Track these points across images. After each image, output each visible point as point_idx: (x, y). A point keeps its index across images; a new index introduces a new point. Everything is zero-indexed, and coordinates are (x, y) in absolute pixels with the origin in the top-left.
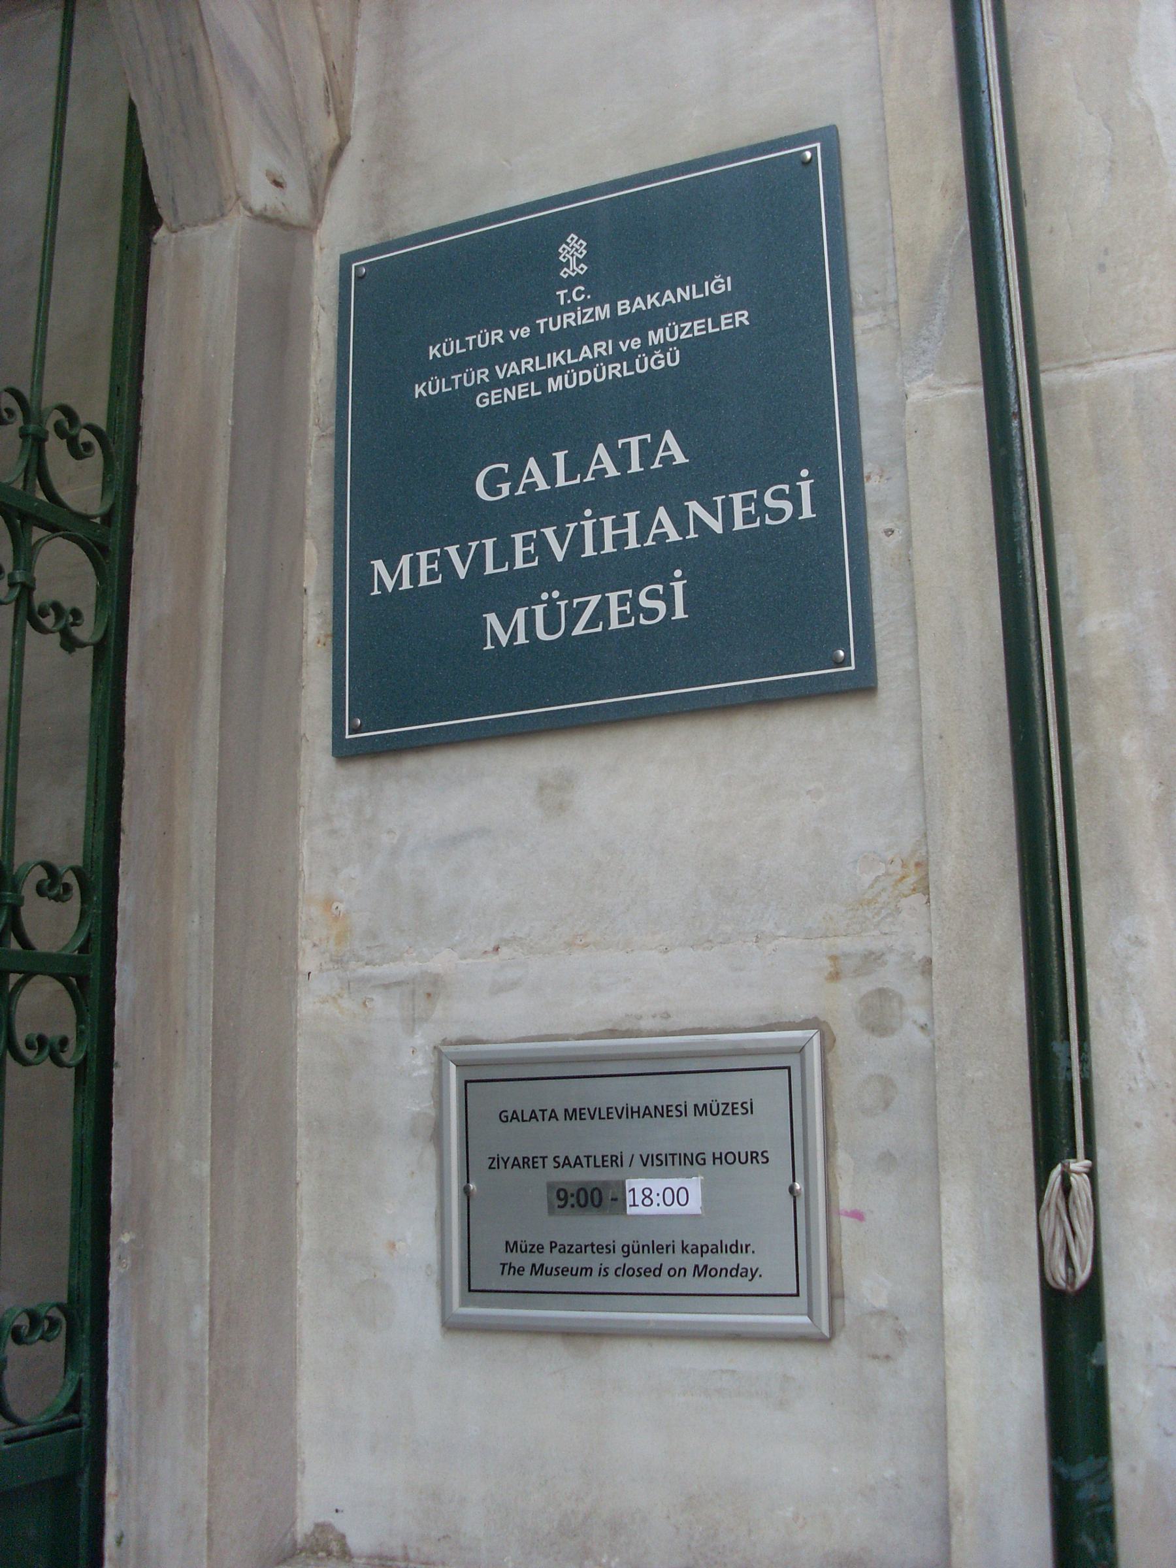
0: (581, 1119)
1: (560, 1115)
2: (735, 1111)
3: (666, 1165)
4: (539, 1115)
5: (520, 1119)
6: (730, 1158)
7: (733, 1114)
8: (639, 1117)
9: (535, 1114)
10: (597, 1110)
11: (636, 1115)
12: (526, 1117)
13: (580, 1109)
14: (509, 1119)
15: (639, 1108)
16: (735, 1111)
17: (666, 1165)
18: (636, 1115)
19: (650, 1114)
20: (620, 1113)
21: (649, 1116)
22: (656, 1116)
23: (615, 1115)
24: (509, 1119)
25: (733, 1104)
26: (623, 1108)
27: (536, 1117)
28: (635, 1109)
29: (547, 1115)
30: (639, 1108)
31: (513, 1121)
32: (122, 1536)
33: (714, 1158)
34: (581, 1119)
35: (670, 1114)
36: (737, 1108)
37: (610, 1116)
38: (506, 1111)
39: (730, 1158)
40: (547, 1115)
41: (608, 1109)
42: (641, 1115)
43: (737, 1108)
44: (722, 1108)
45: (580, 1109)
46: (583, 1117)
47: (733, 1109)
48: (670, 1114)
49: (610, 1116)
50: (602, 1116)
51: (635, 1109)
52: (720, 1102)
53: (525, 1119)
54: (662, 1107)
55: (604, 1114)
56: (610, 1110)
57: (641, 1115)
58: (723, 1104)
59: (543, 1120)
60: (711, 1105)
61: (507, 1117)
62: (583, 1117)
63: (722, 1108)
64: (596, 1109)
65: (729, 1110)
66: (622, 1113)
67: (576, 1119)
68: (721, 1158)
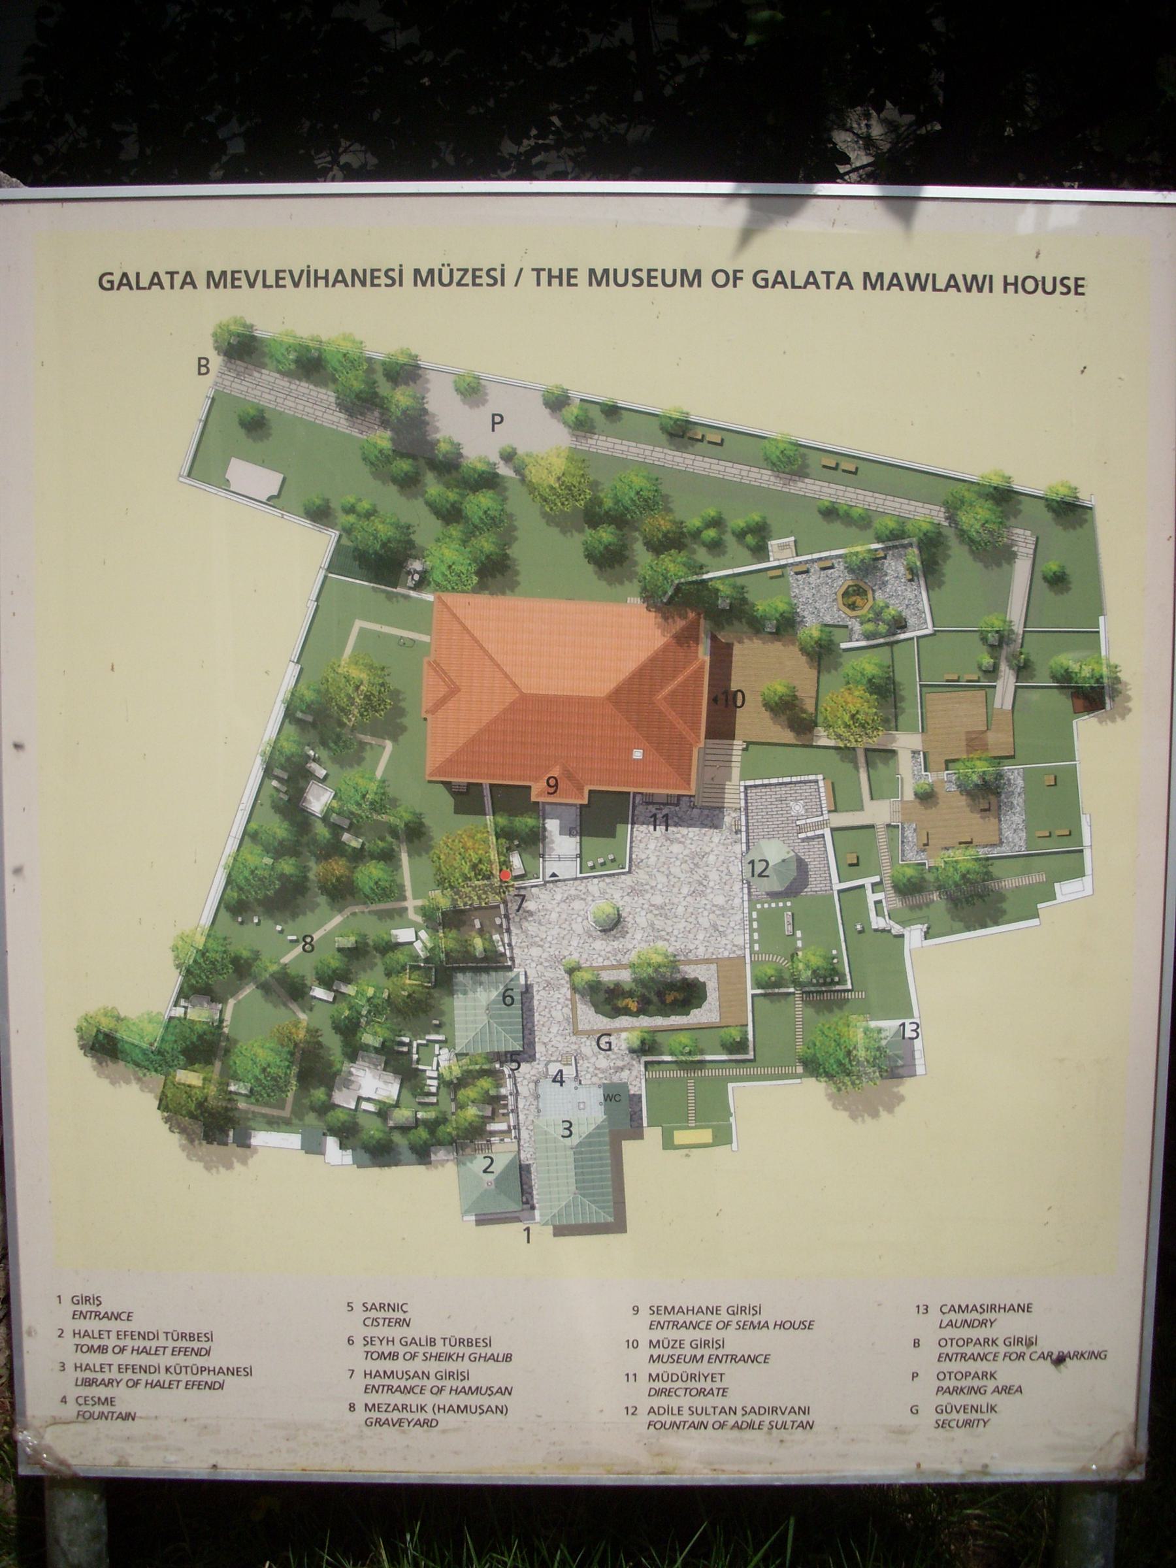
0: (569, 284)
1: (857, 281)
2: (478, 281)
3: (1055, 279)
4: (166, 280)
5: (134, 284)
6: (1030, 285)
7: (474, 284)
8: (327, 285)
9: (815, 278)
10: (261, 274)
11: (321, 283)
12: (144, 282)
13: (233, 273)
14: (770, 283)
15: (327, 271)
16: (478, 281)
17: (1055, 279)
18: (321, 283)
19: (344, 281)
20: (296, 280)
21: (127, 288)
22: (353, 285)
23: (288, 282)
24: (770, 283)
25: (474, 270)
26: (302, 271)
27: (816, 283)
28: (321, 274)
29: (834, 280)
30: (327, 271)
31: (122, 288)
32: (1037, 257)
33: (1006, 284)
34: (233, 286)
35: (376, 281)
36: (379, 277)
37: (281, 282)
38: (766, 272)
39: (1030, 285)
40: (834, 280)
41: (277, 272)
42: (331, 282)
43: (379, 277)
44: (457, 275)
45: (233, 273)
46: (237, 283)
47: (474, 277)
48: (376, 281)
49: (281, 282)
50: (268, 283)
51: (321, 274)
52: (454, 267)
53: (141, 285)
54: (365, 271)
55: (271, 280)
56: (281, 275)
57: (331, 282)
58: (458, 270)
59: (828, 287)
60: (440, 271)
61: (766, 280)
62: (237, 283)
63: (457, 275)
64: (258, 272)
65: (468, 279)
66: (694, 279)
67: (225, 286)
68: (1015, 284)
